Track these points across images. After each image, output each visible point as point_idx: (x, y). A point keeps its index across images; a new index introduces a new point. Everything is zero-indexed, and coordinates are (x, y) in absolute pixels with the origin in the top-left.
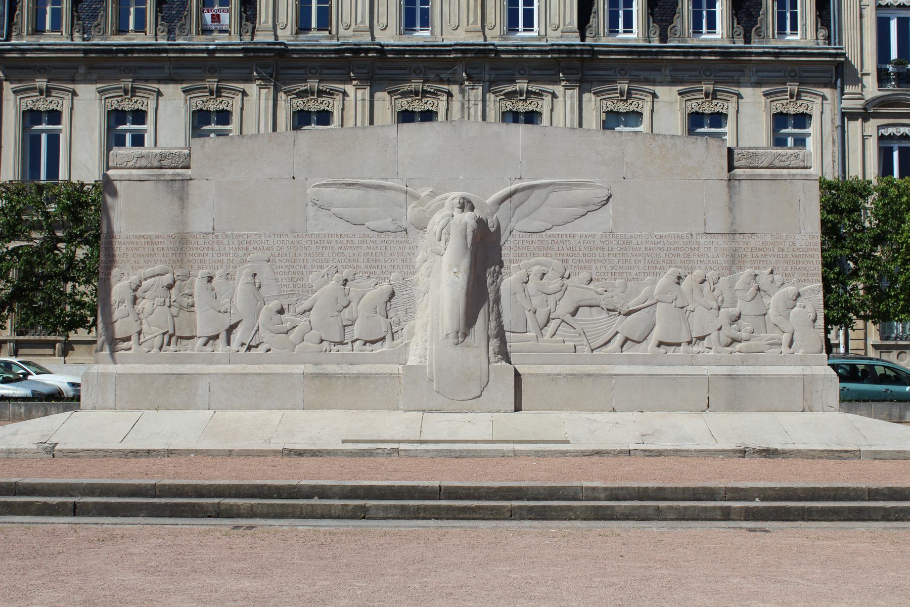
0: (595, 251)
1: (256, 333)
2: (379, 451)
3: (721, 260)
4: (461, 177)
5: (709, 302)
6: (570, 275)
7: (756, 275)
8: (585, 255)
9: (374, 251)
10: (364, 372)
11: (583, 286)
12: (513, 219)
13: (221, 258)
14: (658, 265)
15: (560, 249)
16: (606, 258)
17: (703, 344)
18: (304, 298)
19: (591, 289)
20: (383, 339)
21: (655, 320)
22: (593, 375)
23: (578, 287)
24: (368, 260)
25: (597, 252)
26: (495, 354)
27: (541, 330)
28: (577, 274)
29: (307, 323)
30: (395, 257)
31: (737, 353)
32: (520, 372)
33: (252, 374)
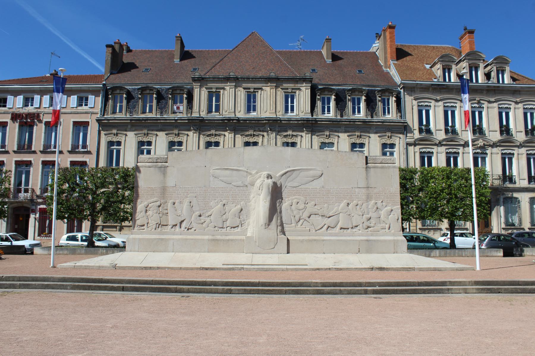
3: (364, 197)
8: (313, 195)
24: (233, 197)
29: (210, 220)
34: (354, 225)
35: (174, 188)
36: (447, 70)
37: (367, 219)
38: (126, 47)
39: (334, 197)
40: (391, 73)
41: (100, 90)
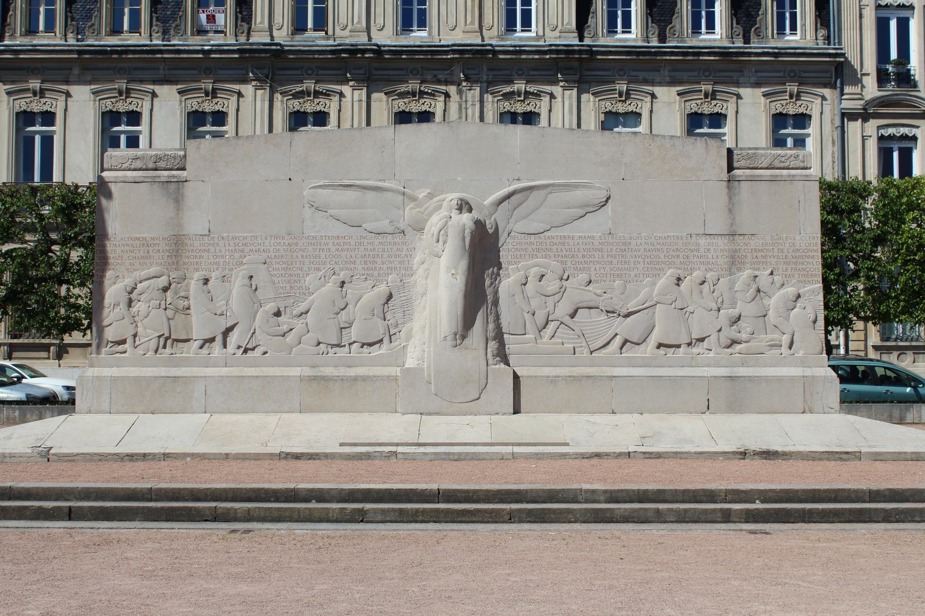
0: (594, 253)
1: (252, 336)
2: (376, 454)
3: (721, 261)
5: (709, 303)
6: (569, 276)
7: (756, 277)
9: (371, 253)
11: (582, 287)
13: (217, 260)
14: (657, 266)
15: (559, 250)
17: (703, 345)
18: (301, 300)
21: (655, 322)
23: (576, 288)
24: (366, 263)
25: (596, 254)
26: (494, 356)
27: (540, 332)
28: (576, 275)
29: (304, 325)
31: (737, 355)
33: (249, 376)
34: (694, 336)
35: (206, 238)
39: (640, 260)
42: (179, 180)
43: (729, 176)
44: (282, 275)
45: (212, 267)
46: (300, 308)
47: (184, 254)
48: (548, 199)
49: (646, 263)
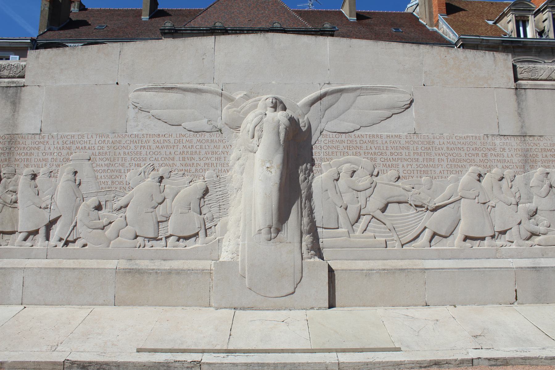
0: (401, 151)
1: (73, 229)
2: (177, 364)
3: (515, 159)
4: (273, 82)
5: (508, 197)
6: (378, 173)
7: (548, 173)
8: (392, 154)
9: (189, 150)
10: (176, 268)
11: (391, 183)
12: (323, 120)
13: (46, 157)
14: (459, 164)
15: (369, 148)
16: (411, 157)
17: (505, 238)
18: (121, 194)
19: (399, 186)
20: (196, 235)
21: (460, 216)
22: (404, 269)
23: (386, 184)
24: (184, 159)
25: (403, 152)
26: (308, 249)
27: (352, 225)
28: (385, 172)
29: (123, 219)
30: (210, 155)
31: (537, 246)
32: (333, 267)
33: (66, 268)
34: (497, 229)
35: (37, 136)
36: (521, 24)
37: (528, 213)
38: (79, 3)
39: (443, 157)
40: (440, 32)
41: (27, 47)
42: (18, 85)
43: (516, 85)
44: (104, 170)
45: (41, 163)
46: (119, 202)
47: (16, 152)
48: (357, 101)
49: (449, 160)
